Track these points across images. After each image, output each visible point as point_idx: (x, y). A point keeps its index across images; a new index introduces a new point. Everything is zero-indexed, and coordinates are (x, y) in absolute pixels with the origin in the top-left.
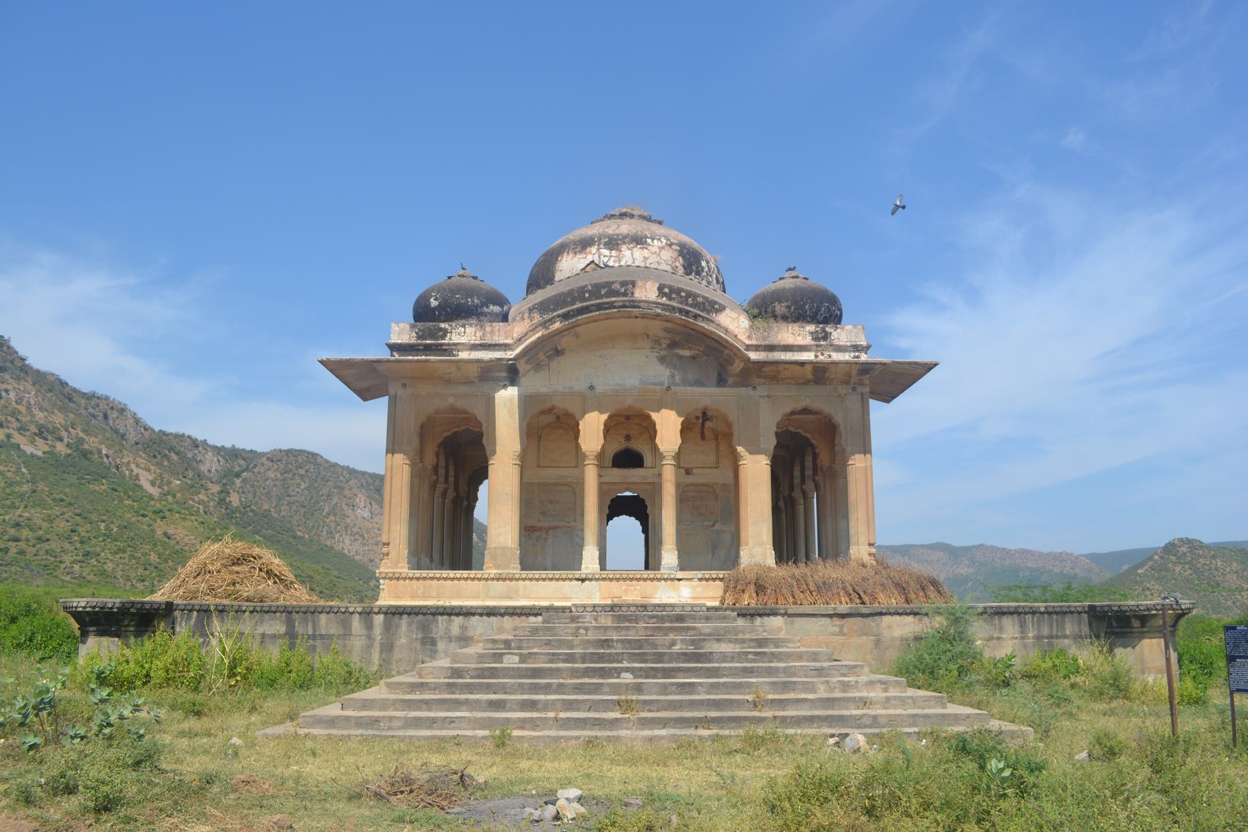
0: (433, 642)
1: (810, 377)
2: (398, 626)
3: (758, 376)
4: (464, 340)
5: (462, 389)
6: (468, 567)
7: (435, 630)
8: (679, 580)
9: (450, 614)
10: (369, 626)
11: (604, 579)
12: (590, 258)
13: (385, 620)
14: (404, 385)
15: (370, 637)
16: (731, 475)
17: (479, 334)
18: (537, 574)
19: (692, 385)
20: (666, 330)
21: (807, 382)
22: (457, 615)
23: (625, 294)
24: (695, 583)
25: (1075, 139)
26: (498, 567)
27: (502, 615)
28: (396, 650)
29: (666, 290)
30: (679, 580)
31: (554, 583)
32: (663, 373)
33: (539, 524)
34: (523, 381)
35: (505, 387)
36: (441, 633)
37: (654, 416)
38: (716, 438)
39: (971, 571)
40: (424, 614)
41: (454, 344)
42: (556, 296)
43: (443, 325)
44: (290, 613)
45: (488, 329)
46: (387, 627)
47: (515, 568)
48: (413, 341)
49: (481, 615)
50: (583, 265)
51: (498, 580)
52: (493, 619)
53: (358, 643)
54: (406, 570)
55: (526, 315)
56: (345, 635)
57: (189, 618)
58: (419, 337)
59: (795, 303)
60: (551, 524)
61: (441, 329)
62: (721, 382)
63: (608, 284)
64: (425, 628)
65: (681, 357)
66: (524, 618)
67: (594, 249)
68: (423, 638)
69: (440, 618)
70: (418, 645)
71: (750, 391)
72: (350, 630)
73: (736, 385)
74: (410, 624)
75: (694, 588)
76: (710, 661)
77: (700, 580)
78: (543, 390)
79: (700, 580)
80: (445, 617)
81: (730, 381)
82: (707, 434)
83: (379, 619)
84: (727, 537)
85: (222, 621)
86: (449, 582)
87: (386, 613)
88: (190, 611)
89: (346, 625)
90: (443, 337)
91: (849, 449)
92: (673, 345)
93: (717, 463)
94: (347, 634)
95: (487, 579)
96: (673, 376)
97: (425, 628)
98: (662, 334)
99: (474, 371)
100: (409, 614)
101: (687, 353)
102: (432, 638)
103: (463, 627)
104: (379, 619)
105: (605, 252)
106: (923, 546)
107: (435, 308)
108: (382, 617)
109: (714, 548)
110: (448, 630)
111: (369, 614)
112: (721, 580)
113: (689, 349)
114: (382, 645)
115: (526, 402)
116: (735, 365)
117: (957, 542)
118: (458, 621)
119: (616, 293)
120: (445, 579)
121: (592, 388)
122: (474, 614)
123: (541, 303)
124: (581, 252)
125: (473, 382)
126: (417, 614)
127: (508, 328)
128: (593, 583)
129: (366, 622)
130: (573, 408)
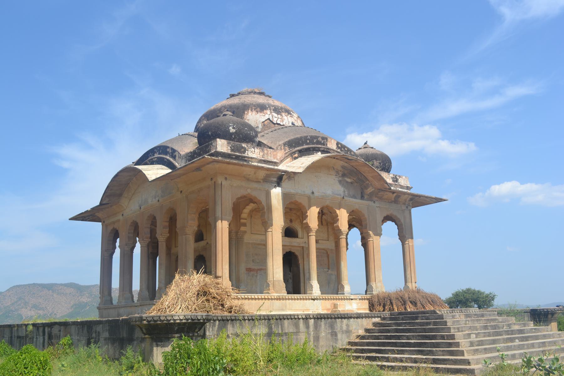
0: (336, 335)
1: (393, 199)
2: (320, 326)
3: (376, 197)
4: (254, 156)
5: (255, 185)
6: (299, 293)
7: (336, 327)
8: (352, 299)
9: (342, 318)
10: (308, 327)
11: (323, 299)
12: (267, 117)
13: (315, 323)
14: (226, 179)
15: (308, 334)
16: (334, 244)
17: (261, 154)
18: (253, 295)
19: (352, 198)
20: (343, 167)
21: (391, 202)
22: (345, 318)
23: (324, 144)
24: (358, 301)
25: (175, 70)
26: (277, 292)
27: (362, 318)
28: (321, 340)
29: (340, 146)
30: (352, 299)
31: (302, 301)
32: (340, 190)
33: (253, 267)
34: (283, 184)
35: (275, 187)
36: (339, 329)
37: (338, 211)
38: (327, 224)
39: (89, 300)
40: (331, 318)
41: (249, 158)
42: (295, 139)
43: (244, 145)
44: (269, 319)
45: (266, 152)
46: (316, 327)
47: (284, 293)
48: (229, 152)
49: (354, 318)
50: (264, 120)
51: (277, 299)
52: (359, 320)
53: (302, 337)
54: (286, 294)
55: (283, 147)
56: (343, 331)
57: (214, 325)
58: (232, 150)
59: (383, 162)
60: (259, 267)
61: (243, 147)
62: (362, 197)
63: (316, 137)
64: (332, 327)
65: (347, 182)
66: (370, 319)
67: (268, 112)
68: (332, 332)
69: (338, 320)
70: (329, 336)
71: (371, 203)
72: (299, 329)
73: (368, 200)
74: (325, 324)
75: (357, 304)
76: (524, 333)
77: (360, 299)
78: (293, 191)
79: (360, 299)
80: (340, 320)
81: (366, 197)
82: (324, 222)
83: (312, 322)
84: (333, 277)
85: (233, 327)
86: (254, 301)
87: (314, 318)
88: (214, 321)
89: (297, 326)
90: (244, 152)
91: (407, 236)
92: (344, 175)
93: (328, 237)
94: (297, 332)
95: (272, 299)
96: (344, 192)
97: (332, 327)
98: (340, 168)
99: (262, 174)
100: (325, 318)
101: (349, 180)
102: (335, 332)
103: (348, 325)
104: (312, 322)
105: (275, 115)
106: (61, 285)
107: (232, 134)
108: (313, 320)
109: (329, 283)
110: (341, 327)
111: (307, 319)
112: (367, 299)
113: (350, 178)
114: (314, 337)
115: (285, 196)
116: (369, 190)
117: (82, 283)
118: (345, 321)
119: (318, 143)
120: (252, 299)
121: (313, 193)
122: (351, 318)
123: (289, 142)
124: (261, 112)
125: (260, 182)
126: (328, 318)
127: (275, 153)
128: (319, 301)
129: (306, 324)
130: (305, 203)
